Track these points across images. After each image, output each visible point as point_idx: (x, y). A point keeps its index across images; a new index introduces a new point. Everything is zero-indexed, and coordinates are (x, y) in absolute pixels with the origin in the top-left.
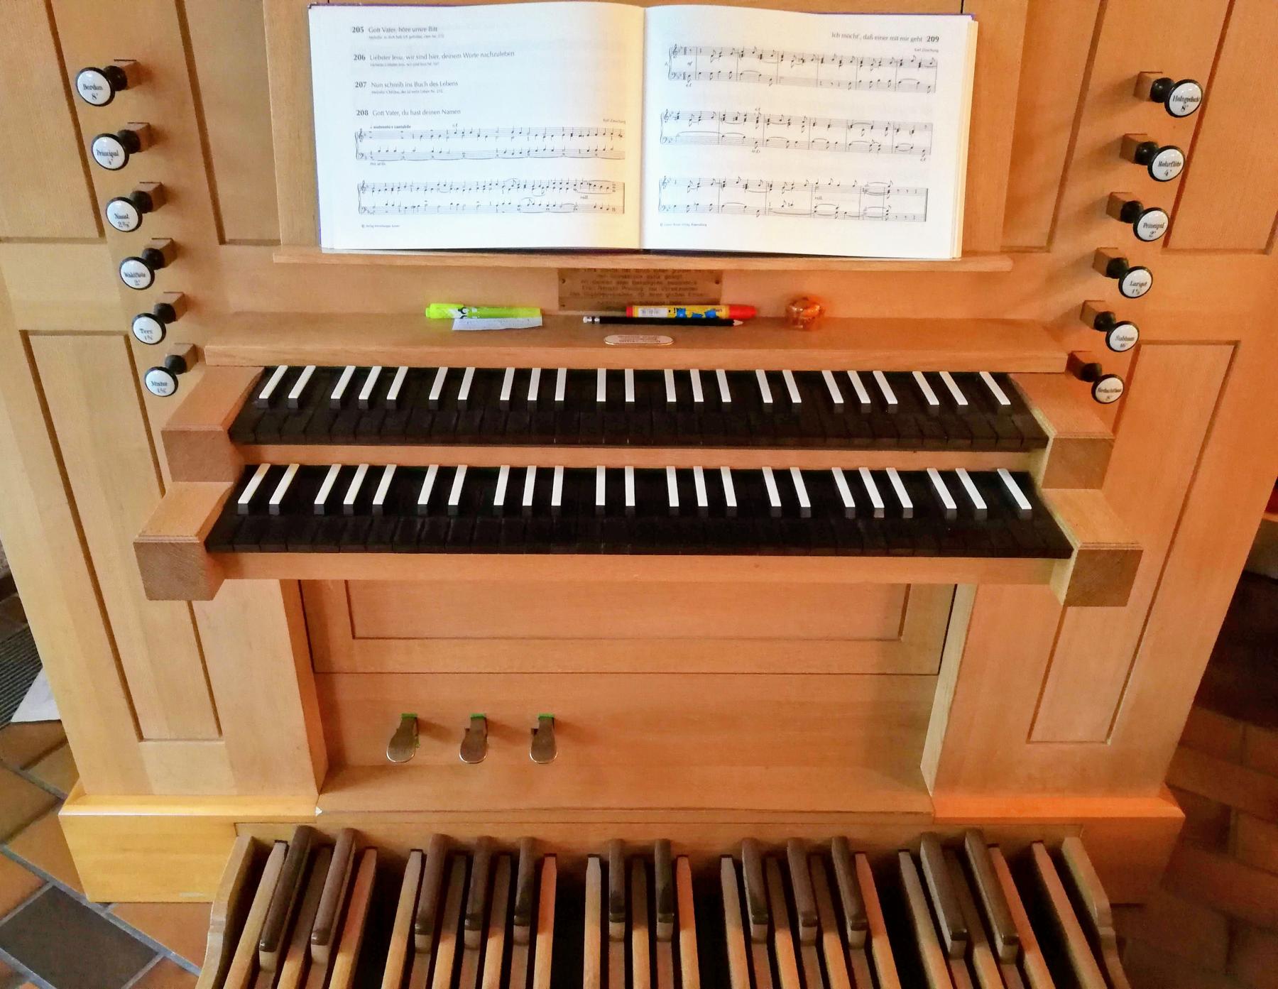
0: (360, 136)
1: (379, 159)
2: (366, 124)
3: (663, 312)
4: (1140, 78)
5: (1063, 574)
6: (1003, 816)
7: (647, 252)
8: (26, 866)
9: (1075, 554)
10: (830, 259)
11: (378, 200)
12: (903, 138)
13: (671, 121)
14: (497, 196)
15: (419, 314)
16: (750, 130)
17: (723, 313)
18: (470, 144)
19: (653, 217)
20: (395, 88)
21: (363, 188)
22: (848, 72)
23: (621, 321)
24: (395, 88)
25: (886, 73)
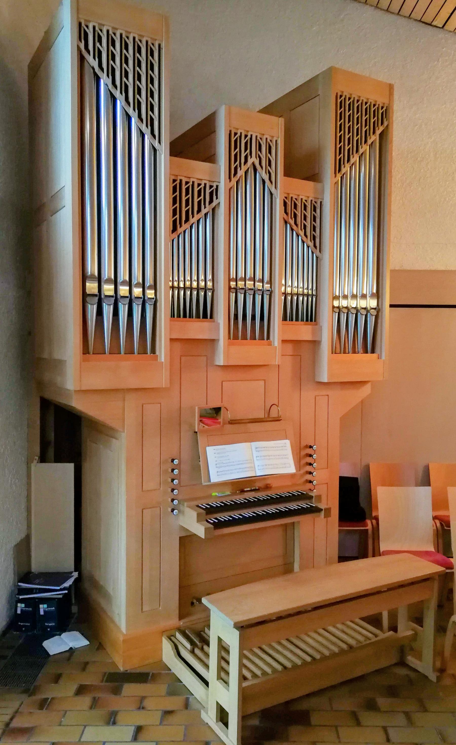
0: (216, 464)
1: (219, 467)
2: (217, 463)
3: (249, 489)
4: (307, 445)
5: (323, 513)
6: (394, 121)
7: (257, 476)
8: (47, 742)
9: (323, 510)
10: (273, 476)
11: (220, 473)
12: (285, 457)
13: (258, 457)
14: (238, 470)
15: (211, 495)
16: (268, 457)
17: (257, 488)
18: (232, 464)
19: (257, 471)
20: (221, 457)
21: (218, 472)
22: (277, 448)
23: (243, 491)
24: (221, 457)
25: (280, 448)
